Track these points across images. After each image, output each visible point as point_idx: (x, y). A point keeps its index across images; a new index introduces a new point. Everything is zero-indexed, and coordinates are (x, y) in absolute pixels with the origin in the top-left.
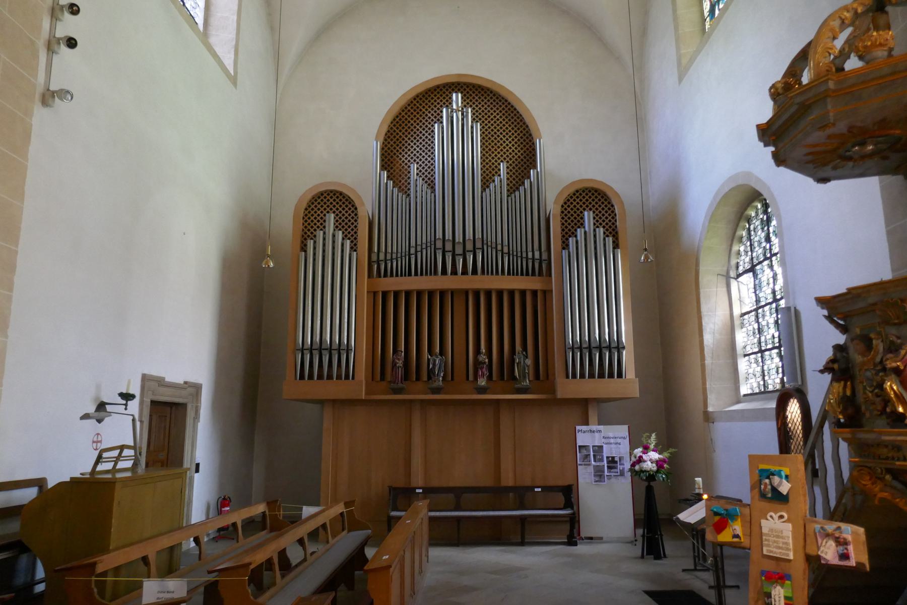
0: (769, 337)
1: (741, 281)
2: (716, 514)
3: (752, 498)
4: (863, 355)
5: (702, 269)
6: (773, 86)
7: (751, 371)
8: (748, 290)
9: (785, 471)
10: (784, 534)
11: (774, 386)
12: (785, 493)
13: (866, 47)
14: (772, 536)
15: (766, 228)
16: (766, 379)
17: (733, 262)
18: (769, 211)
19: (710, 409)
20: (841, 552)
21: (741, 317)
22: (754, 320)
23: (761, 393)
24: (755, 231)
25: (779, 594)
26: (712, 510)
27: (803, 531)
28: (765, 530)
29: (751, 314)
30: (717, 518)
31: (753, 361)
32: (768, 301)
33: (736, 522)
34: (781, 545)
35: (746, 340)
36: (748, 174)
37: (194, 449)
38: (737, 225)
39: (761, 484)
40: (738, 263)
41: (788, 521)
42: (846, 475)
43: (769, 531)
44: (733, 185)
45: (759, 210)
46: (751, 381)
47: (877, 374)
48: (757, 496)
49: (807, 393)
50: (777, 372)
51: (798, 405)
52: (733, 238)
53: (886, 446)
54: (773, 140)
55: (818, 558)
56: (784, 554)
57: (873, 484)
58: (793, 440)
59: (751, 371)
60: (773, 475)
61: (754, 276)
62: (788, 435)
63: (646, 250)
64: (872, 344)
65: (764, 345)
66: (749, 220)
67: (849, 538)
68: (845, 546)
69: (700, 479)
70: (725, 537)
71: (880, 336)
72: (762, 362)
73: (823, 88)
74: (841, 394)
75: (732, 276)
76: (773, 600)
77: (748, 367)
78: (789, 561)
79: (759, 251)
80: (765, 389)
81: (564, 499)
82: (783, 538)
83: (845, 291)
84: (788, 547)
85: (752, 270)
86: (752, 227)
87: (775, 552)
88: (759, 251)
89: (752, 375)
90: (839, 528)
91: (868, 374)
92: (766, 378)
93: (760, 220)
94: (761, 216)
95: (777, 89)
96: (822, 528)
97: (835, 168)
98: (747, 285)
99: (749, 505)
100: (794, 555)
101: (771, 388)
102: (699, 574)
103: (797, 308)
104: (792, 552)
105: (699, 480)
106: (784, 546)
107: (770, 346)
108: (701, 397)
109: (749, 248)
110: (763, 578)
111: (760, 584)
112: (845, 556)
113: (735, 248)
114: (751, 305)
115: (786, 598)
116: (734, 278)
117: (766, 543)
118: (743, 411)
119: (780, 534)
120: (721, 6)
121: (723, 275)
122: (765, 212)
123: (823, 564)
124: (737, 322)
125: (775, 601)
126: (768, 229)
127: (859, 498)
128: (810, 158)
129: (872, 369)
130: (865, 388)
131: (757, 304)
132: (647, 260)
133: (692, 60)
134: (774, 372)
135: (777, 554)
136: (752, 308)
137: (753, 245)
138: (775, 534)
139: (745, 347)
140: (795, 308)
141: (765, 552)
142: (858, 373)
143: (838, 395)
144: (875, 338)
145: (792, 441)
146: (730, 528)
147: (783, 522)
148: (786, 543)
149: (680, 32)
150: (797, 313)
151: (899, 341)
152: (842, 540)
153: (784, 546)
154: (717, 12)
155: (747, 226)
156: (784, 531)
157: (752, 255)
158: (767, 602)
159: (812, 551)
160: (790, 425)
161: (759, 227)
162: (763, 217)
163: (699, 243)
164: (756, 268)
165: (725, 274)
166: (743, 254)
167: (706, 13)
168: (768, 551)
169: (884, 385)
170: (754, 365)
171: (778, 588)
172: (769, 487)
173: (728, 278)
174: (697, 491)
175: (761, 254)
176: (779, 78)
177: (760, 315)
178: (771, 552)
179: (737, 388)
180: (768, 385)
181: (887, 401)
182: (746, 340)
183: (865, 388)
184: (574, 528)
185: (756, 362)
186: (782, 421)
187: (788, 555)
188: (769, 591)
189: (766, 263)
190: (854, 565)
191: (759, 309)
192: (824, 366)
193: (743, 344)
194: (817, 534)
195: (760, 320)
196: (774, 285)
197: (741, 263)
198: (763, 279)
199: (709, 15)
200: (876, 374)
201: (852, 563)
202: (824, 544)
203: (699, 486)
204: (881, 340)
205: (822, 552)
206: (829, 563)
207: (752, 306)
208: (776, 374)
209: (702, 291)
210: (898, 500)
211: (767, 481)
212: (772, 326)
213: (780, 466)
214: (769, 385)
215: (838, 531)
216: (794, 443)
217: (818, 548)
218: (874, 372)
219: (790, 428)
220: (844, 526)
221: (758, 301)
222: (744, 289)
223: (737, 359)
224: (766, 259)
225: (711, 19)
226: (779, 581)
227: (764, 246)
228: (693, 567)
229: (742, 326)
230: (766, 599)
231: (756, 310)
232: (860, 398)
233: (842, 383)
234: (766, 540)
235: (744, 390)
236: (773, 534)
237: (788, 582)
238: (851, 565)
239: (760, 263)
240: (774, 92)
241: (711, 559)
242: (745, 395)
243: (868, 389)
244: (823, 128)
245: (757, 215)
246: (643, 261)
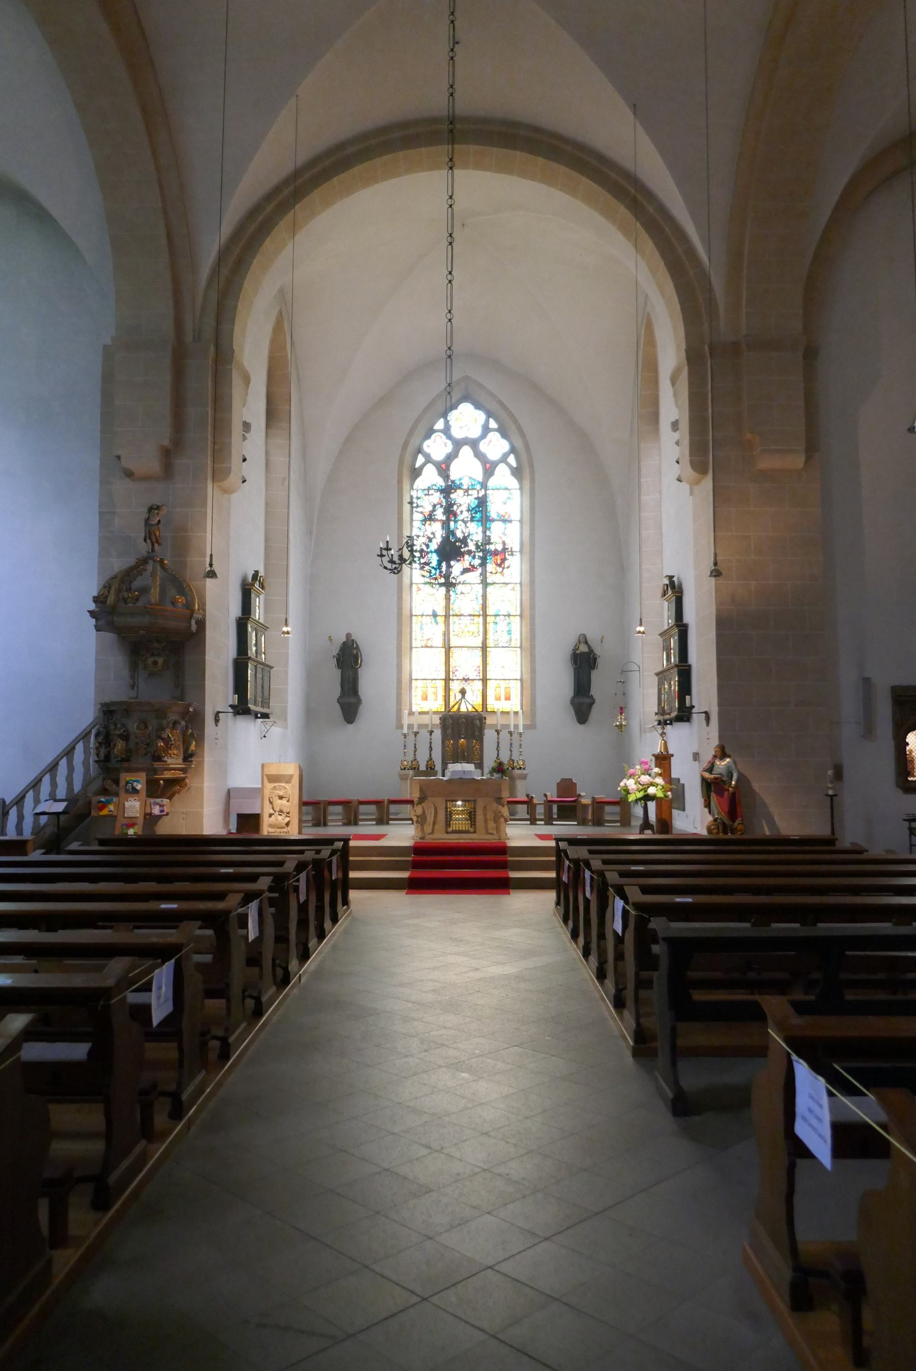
41: (138, 801)
42: (77, 786)
70: (105, 812)
78: (137, 817)
81: (234, 347)
141: (126, 816)
159: (148, 811)
168: (127, 815)
172: (131, 787)
184: (158, 882)
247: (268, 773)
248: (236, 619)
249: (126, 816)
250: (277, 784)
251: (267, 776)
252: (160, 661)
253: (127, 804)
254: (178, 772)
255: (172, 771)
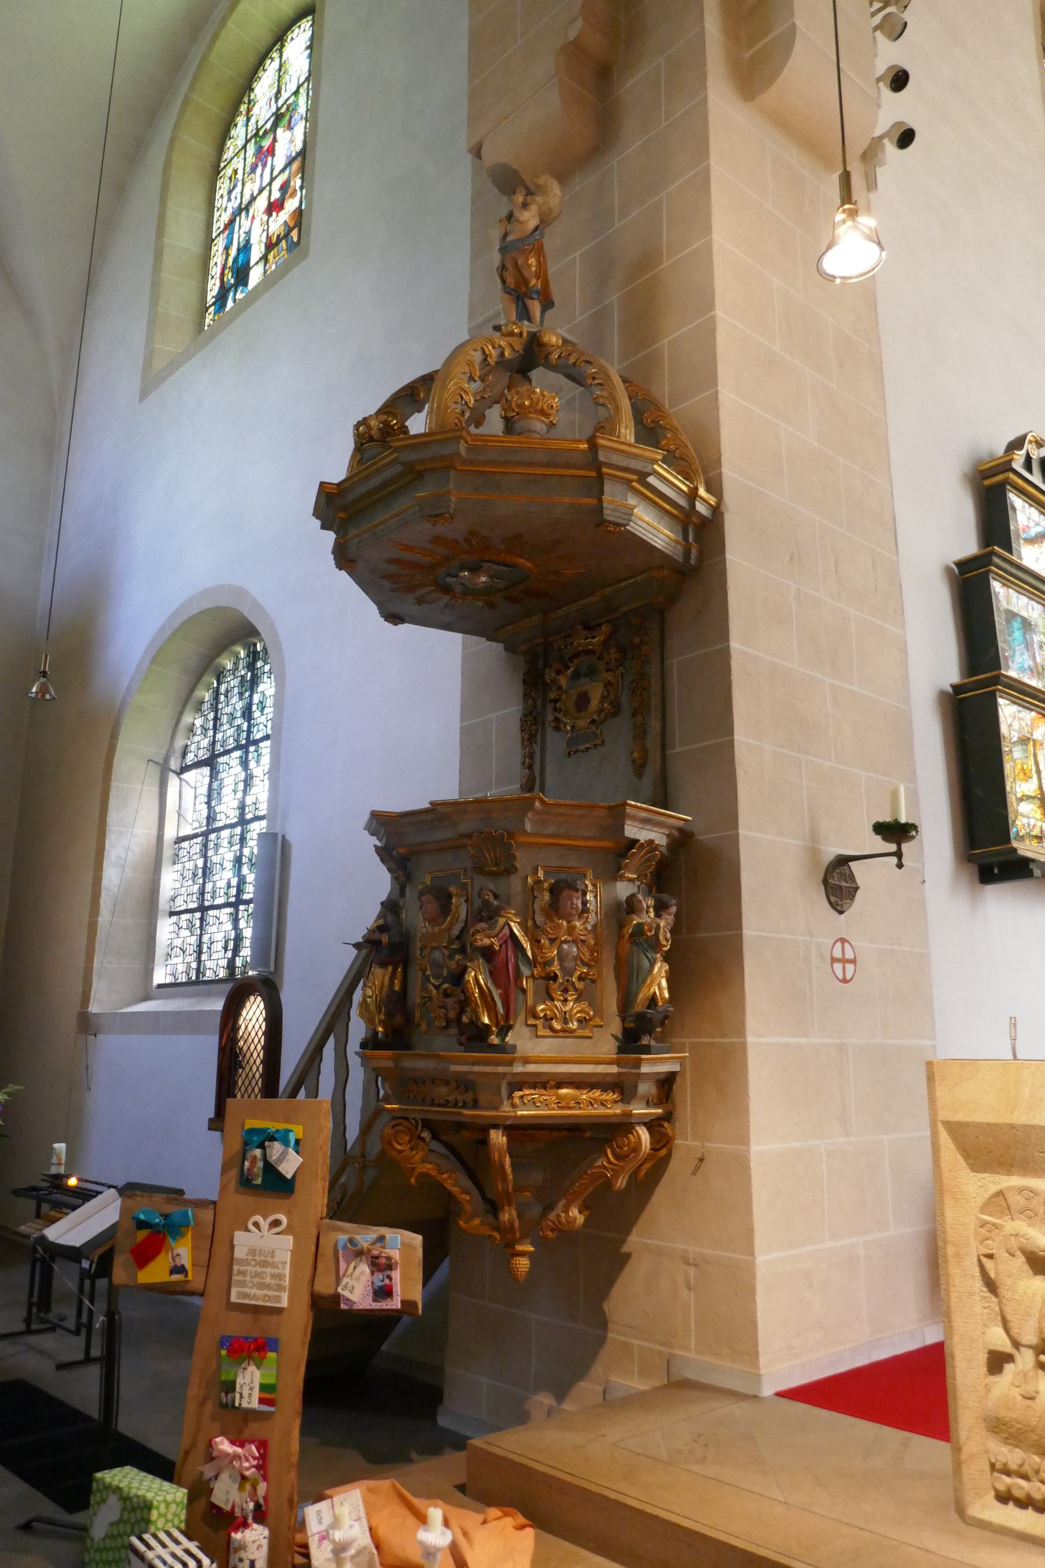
0: (221, 884)
1: (186, 779)
2: (141, 1225)
3: (223, 1188)
4: (432, 921)
5: (122, 745)
6: (364, 421)
7: (178, 942)
8: (196, 798)
9: (297, 1131)
10: (278, 1258)
11: (215, 973)
12: (289, 1176)
13: (521, 406)
14: (253, 1263)
15: (247, 694)
16: (203, 959)
17: (179, 743)
18: (259, 666)
19: (94, 1008)
20: (380, 1284)
21: (176, 843)
22: (198, 851)
23: (189, 983)
24: (226, 696)
25: (252, 1382)
26: (134, 1218)
27: (313, 1247)
28: (239, 1253)
29: (195, 840)
30: (142, 1234)
31: (184, 925)
32: (229, 822)
33: (183, 1240)
34: (268, 1280)
35: (178, 885)
36: (240, 592)
37: (346, 985)
38: (199, 679)
39: (244, 1159)
40: (187, 746)
43: (247, 1255)
44: (207, 604)
45: (241, 661)
46: (175, 960)
47: (451, 957)
48: (233, 1184)
49: (282, 988)
50: (226, 949)
51: (262, 1006)
52: (187, 701)
53: (447, 1083)
54: (341, 518)
55: (337, 1298)
56: (270, 1298)
57: (412, 1149)
58: (244, 1069)
59: (178, 942)
60: (272, 1139)
61: (211, 776)
62: (236, 1061)
63: (44, 674)
64: (451, 902)
65: (209, 898)
66: (220, 675)
67: (396, 1255)
68: (388, 1272)
69: (63, 1145)
70: (156, 1272)
71: (465, 892)
72: (201, 928)
73: (449, 450)
74: (385, 989)
75: (173, 767)
76: (238, 1396)
77: (174, 935)
78: (279, 1311)
79: (227, 733)
80: (197, 976)
82: (274, 1265)
83: (426, 805)
84: (282, 1282)
85: (210, 762)
86: (223, 688)
87: (254, 1295)
88: (227, 733)
89: (178, 949)
90: (381, 1239)
91: (437, 955)
92: (204, 957)
93: (240, 678)
94: (243, 673)
95: (369, 428)
96: (351, 1241)
97: (420, 601)
98: (195, 788)
99: (214, 1203)
100: (291, 1299)
101: (209, 975)
102: (32, 1340)
103: (287, 837)
104: (287, 1293)
105: (60, 1147)
106: (273, 1282)
107: (219, 901)
108: (79, 988)
109: (211, 723)
110: (224, 1352)
111: (214, 1366)
112: (384, 1292)
113: (187, 719)
114: (196, 825)
115: (263, 1388)
116: (174, 772)
117: (240, 1278)
118: (156, 1015)
119: (268, 1259)
120: (240, 296)
121: (157, 763)
122: (251, 666)
123: (345, 1310)
124: (167, 852)
125: (241, 1397)
126: (251, 696)
127: (371, 1174)
128: (393, 569)
129: (445, 947)
130: (426, 979)
131: (208, 825)
132: (43, 696)
133: (174, 365)
134: (219, 946)
135: (257, 1300)
136: (199, 831)
137: (220, 720)
138: (258, 1259)
139: (173, 899)
140: (283, 836)
141: (234, 1299)
142: (418, 952)
143: (381, 991)
144: (456, 895)
145: (240, 1071)
146: (167, 1253)
147: (277, 1234)
148: (279, 1277)
149: (159, 310)
150: (285, 845)
151: (496, 903)
152: (383, 1261)
153: (273, 1282)
154: (230, 304)
155: (215, 685)
156: (277, 1253)
157: (214, 736)
158: (224, 1401)
159: (324, 1287)
160: (241, 1043)
161: (236, 690)
162: (247, 674)
163: (124, 698)
164: (218, 760)
165: (161, 761)
166: (199, 732)
167: (210, 300)
169: (466, 976)
170: (185, 933)
171: (252, 1368)
172: (260, 1164)
173: (164, 770)
174: (54, 1170)
175: (232, 738)
176: (372, 410)
177: (211, 845)
178: (246, 1296)
179: (149, 973)
180: (205, 969)
181: (465, 1003)
182: (178, 885)
183: (426, 979)
185: (191, 927)
186: (229, 1035)
187: (278, 1299)
188: (231, 1377)
189: (237, 754)
190: (399, 1307)
191: (210, 833)
192: (363, 937)
193: (172, 894)
194: (340, 1252)
195: (210, 853)
196: (245, 792)
197: (193, 747)
198: (226, 782)
199: (214, 304)
200: (449, 956)
201: (395, 1303)
202: (349, 1273)
203: (60, 1159)
204: (465, 898)
205: (345, 1287)
206: (355, 1307)
207: (198, 826)
208: (223, 951)
209: (114, 784)
210: (445, 1176)
211: (258, 1152)
212: (228, 865)
213: (287, 1121)
214: (208, 971)
215: (379, 1245)
216: (244, 1076)
217: (338, 1281)
218: (446, 953)
219: (241, 1049)
220: (388, 1233)
221: (211, 818)
222: (188, 794)
223: (156, 919)
224: (238, 747)
225: (216, 312)
226: (255, 1355)
227: (239, 723)
228: (22, 1327)
229: (176, 859)
230: (223, 1394)
231: (205, 834)
232: (415, 997)
233: (390, 968)
234: (240, 1272)
235: (160, 976)
236: (255, 1260)
237: (272, 1355)
238: (394, 1307)
239: (227, 752)
240: (365, 433)
241: (102, 1318)
242: (160, 986)
243: (432, 981)
244: (435, 518)
245: (236, 668)
246: (33, 695)
247: (960, 1117)
248: (948, 570)
249: (234, 1299)
250: (1015, 1181)
251: (956, 1129)
252: (596, 693)
253: (243, 1242)
254: (596, 1093)
255: (564, 1091)
